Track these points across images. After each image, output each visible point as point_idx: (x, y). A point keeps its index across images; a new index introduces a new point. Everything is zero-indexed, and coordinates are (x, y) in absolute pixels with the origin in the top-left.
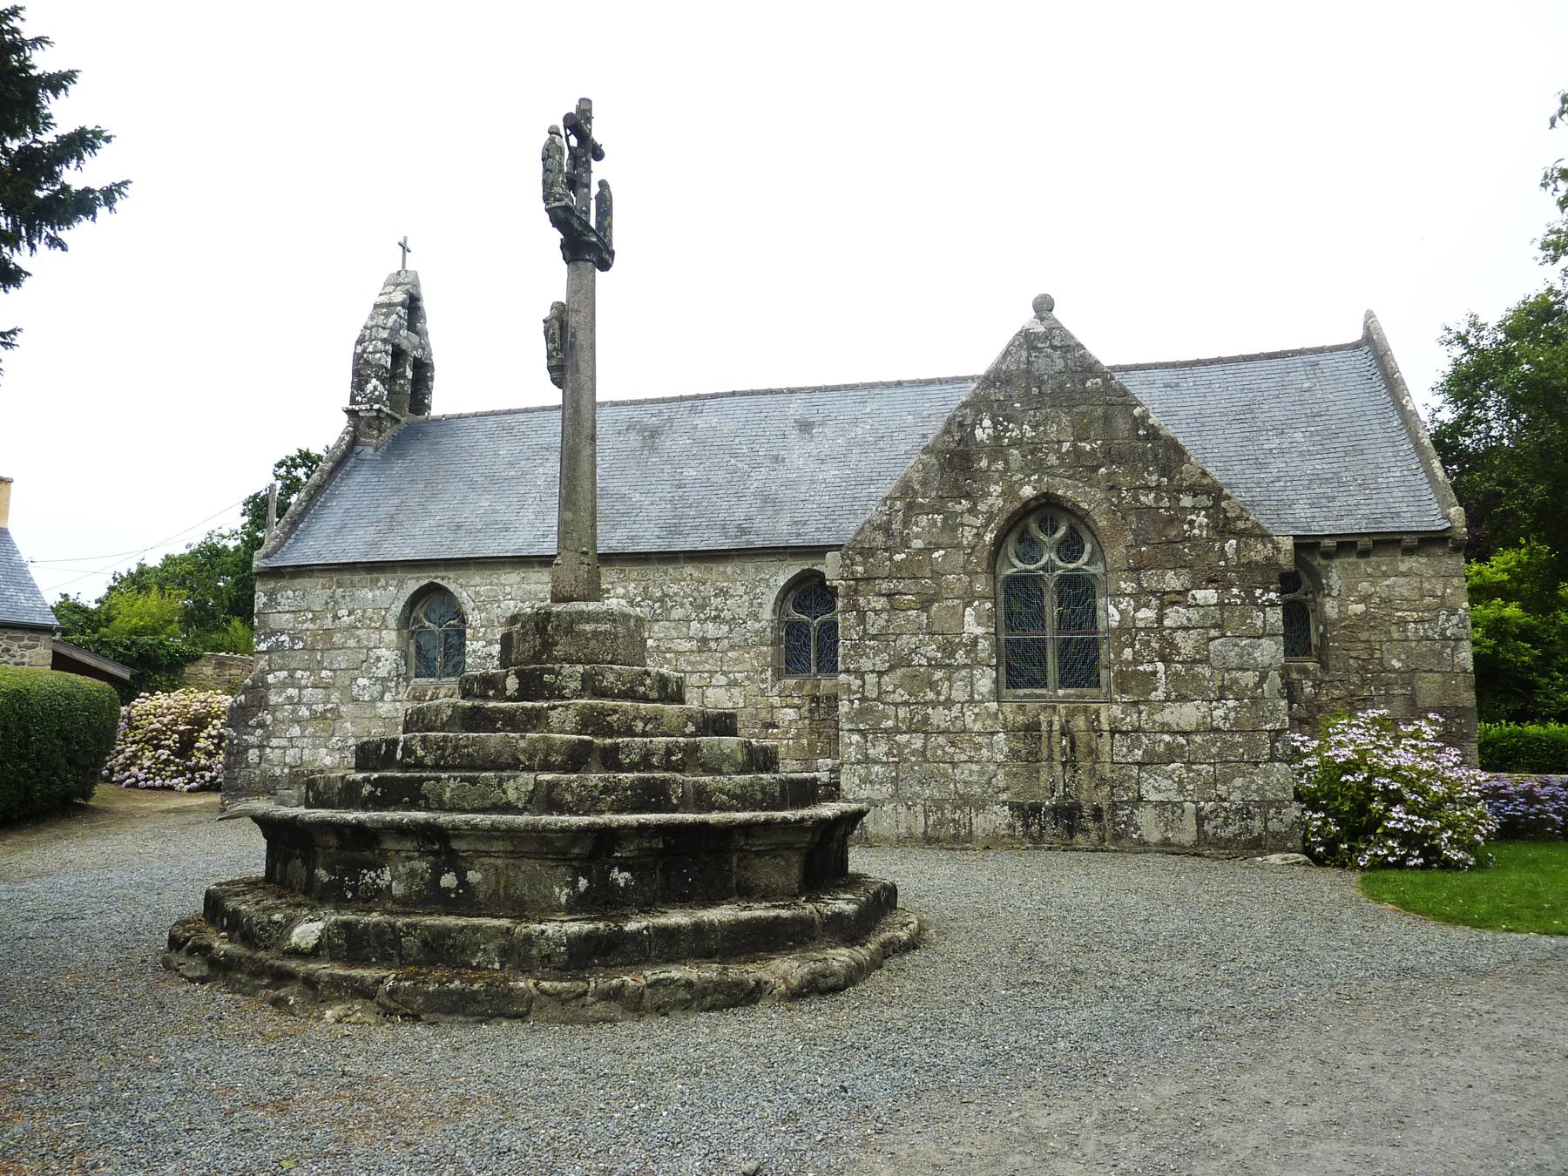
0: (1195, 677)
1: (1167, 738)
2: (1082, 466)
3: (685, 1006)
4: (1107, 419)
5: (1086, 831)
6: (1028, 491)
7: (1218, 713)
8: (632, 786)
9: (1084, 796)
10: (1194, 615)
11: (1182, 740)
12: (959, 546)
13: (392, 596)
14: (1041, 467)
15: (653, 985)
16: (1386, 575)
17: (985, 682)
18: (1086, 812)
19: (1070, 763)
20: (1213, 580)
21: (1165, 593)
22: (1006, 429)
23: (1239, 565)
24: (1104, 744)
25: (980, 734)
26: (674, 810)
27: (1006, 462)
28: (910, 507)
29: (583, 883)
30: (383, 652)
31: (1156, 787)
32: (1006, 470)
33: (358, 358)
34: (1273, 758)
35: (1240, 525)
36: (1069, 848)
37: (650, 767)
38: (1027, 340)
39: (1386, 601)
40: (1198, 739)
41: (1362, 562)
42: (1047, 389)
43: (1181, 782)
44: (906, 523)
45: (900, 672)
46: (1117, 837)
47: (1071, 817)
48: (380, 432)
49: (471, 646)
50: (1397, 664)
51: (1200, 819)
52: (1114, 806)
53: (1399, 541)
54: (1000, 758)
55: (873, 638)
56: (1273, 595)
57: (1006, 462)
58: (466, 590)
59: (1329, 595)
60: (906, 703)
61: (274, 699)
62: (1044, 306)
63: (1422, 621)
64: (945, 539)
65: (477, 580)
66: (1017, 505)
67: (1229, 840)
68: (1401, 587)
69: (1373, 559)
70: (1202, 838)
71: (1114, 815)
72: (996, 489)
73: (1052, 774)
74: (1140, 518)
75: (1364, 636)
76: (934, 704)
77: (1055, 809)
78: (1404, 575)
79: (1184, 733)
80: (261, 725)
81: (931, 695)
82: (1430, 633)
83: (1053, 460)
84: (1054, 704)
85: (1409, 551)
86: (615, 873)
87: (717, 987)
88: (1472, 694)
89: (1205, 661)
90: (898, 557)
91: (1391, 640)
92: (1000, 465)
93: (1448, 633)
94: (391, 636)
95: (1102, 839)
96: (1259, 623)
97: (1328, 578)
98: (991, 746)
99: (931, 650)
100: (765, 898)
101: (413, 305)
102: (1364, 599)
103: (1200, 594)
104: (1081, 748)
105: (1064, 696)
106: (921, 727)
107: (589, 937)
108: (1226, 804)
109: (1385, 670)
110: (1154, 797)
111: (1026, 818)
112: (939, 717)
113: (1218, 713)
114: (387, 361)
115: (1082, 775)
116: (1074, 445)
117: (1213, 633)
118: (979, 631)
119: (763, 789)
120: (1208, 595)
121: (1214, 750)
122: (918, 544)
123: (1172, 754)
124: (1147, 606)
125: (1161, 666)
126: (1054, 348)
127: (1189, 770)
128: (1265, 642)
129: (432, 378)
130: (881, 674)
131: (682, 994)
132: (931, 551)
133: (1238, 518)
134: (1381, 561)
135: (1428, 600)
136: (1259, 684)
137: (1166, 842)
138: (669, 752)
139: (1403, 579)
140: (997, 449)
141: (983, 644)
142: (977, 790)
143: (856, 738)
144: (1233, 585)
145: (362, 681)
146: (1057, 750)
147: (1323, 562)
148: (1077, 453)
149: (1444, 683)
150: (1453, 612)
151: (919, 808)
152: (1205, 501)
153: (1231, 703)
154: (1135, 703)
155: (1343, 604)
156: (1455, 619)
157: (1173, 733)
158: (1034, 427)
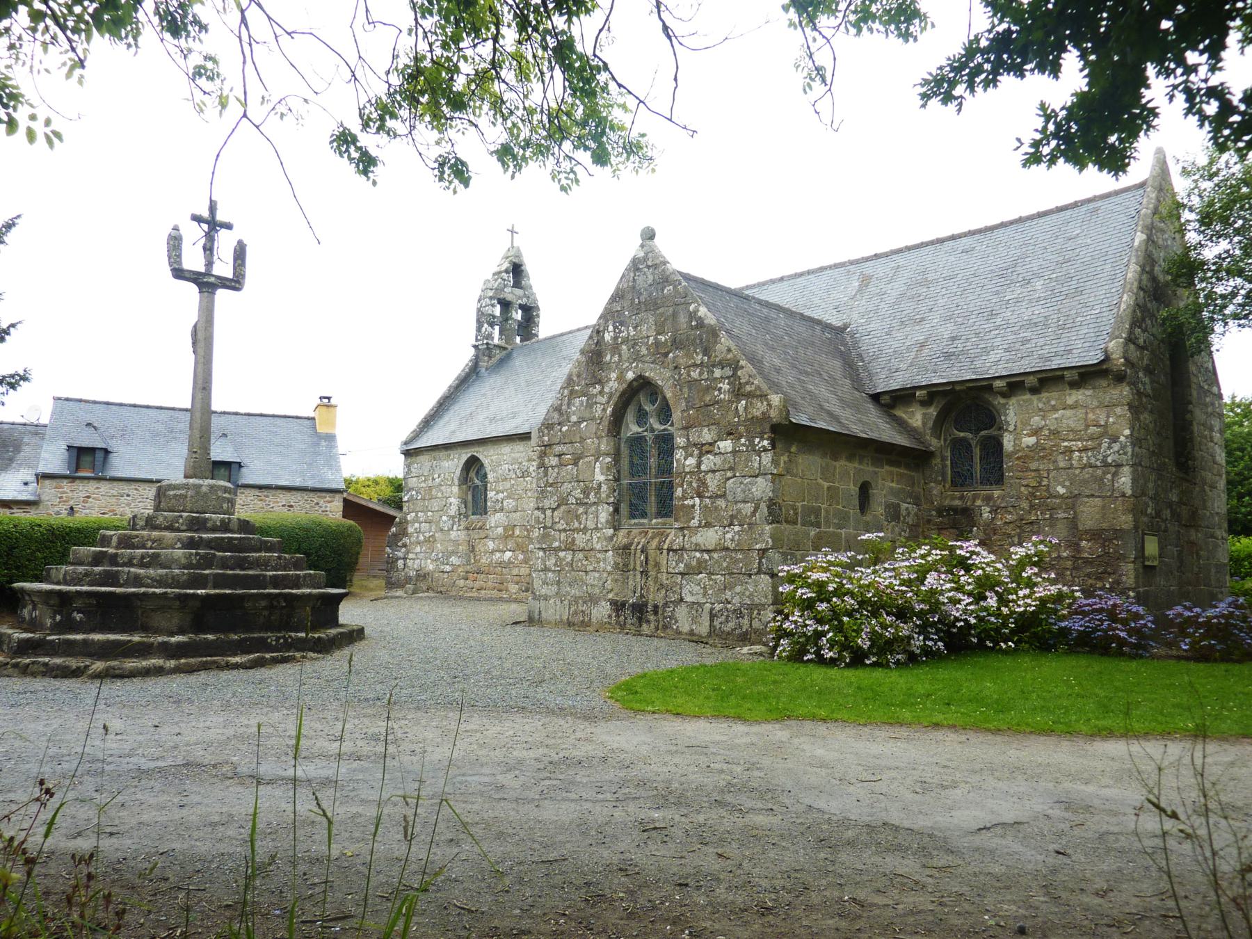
0: (716, 508)
1: (698, 555)
2: (660, 353)
3: (44, 675)
4: (675, 315)
5: (648, 622)
6: (630, 375)
7: (729, 536)
8: (100, 574)
9: (651, 597)
10: (718, 460)
11: (706, 556)
12: (593, 419)
13: (453, 464)
14: (637, 358)
15: (34, 663)
16: (1054, 409)
17: (604, 513)
18: (650, 608)
19: (644, 573)
20: (730, 434)
21: (703, 445)
22: (620, 332)
23: (747, 420)
24: (663, 559)
25: (599, 551)
26: (121, 586)
27: (620, 356)
28: (572, 392)
29: (58, 618)
30: (452, 500)
31: (691, 591)
32: (620, 361)
33: (479, 310)
34: (759, 572)
35: (748, 388)
36: (639, 634)
37: (132, 565)
38: (635, 265)
39: (1055, 433)
40: (715, 555)
41: (1035, 398)
42: (643, 299)
43: (705, 588)
44: (569, 405)
45: (563, 508)
46: (665, 627)
47: (641, 612)
48: (490, 357)
49: (491, 494)
50: (1061, 490)
51: (712, 616)
52: (666, 605)
53: (1062, 377)
54: (609, 568)
55: (551, 485)
56: (765, 443)
57: (620, 356)
58: (488, 457)
59: (1007, 430)
60: (565, 530)
61: (410, 530)
62: (649, 235)
63: (1086, 449)
64: (587, 415)
65: (492, 452)
66: (625, 386)
67: (728, 633)
68: (1066, 419)
69: (1045, 395)
70: (713, 631)
71: (664, 611)
72: (613, 375)
73: (635, 580)
74: (690, 389)
75: (1034, 465)
76: (578, 530)
77: (633, 605)
78: (1072, 407)
79: (708, 551)
80: (405, 546)
81: (576, 525)
82: (1093, 461)
83: (644, 351)
84: (636, 532)
85: (1075, 385)
86: (75, 614)
87: (58, 667)
88: (1130, 518)
89: (724, 496)
90: (565, 429)
91: (1058, 469)
92: (616, 358)
93: (1109, 460)
94: (455, 489)
95: (657, 628)
96: (756, 465)
97: (1006, 415)
98: (605, 560)
99: (578, 493)
100: (155, 633)
101: (517, 270)
102: (1036, 432)
103: (722, 444)
104: (651, 562)
105: (657, 524)
106: (570, 547)
107: (28, 640)
108: (729, 606)
109: (1051, 496)
110: (689, 599)
111: (617, 611)
112: (580, 539)
113: (729, 536)
114: (497, 311)
115: (651, 582)
116: (656, 339)
117: (729, 474)
118: (602, 478)
119: (173, 577)
120: (726, 445)
121: (725, 564)
122: (574, 419)
123: (700, 567)
124: (691, 455)
125: (697, 500)
126: (648, 267)
127: (710, 579)
128: (759, 479)
129: (538, 316)
130: (554, 510)
131: (43, 669)
132: (580, 422)
133: (747, 383)
134: (1052, 396)
135: (1092, 430)
136: (754, 513)
137: (692, 633)
138: (143, 557)
139: (1070, 413)
140: (616, 348)
141: (604, 487)
142: (597, 591)
143: (541, 553)
144: (741, 436)
145: (444, 518)
146: (638, 563)
147: (1002, 401)
148: (657, 343)
149: (1104, 507)
150: (1114, 439)
151: (566, 602)
152: (728, 372)
153: (737, 528)
154: (682, 529)
155: (1017, 439)
156: (1116, 447)
157: (702, 551)
158: (635, 328)
